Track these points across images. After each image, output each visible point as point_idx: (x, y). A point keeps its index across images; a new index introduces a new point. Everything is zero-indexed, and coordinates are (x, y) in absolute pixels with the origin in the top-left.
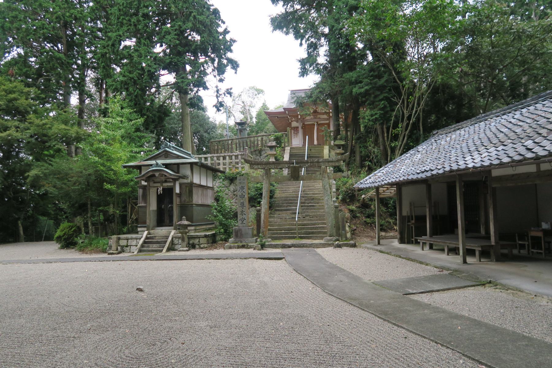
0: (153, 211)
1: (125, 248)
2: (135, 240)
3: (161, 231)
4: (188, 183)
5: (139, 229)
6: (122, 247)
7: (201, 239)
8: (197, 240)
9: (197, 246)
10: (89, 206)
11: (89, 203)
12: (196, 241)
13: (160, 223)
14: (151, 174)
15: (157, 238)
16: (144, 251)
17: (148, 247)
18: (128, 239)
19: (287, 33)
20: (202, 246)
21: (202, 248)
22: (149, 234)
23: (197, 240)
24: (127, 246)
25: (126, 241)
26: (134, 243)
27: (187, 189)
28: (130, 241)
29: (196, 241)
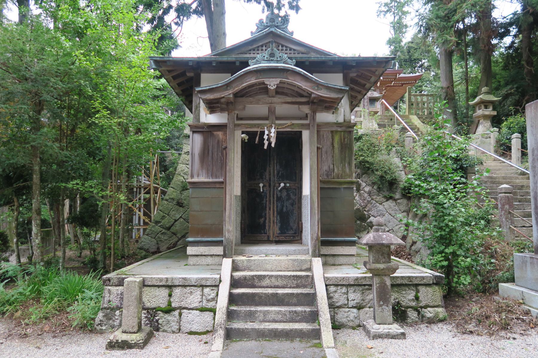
0: (236, 196)
1: (161, 318)
2: (198, 292)
3: (271, 260)
4: (338, 124)
5: (190, 250)
6: (152, 312)
7: (422, 289)
8: (411, 295)
9: (412, 315)
10: (36, 178)
11: (37, 168)
12: (407, 297)
13: (253, 232)
14: (253, 80)
15: (266, 282)
16: (243, 334)
17: (251, 316)
18: (170, 287)
19: (292, 33)
20: (429, 313)
21: (431, 321)
22: (235, 268)
23: (411, 295)
24: (169, 310)
25: (165, 292)
26: (194, 298)
27: (337, 139)
28: (177, 291)
29: (407, 297)
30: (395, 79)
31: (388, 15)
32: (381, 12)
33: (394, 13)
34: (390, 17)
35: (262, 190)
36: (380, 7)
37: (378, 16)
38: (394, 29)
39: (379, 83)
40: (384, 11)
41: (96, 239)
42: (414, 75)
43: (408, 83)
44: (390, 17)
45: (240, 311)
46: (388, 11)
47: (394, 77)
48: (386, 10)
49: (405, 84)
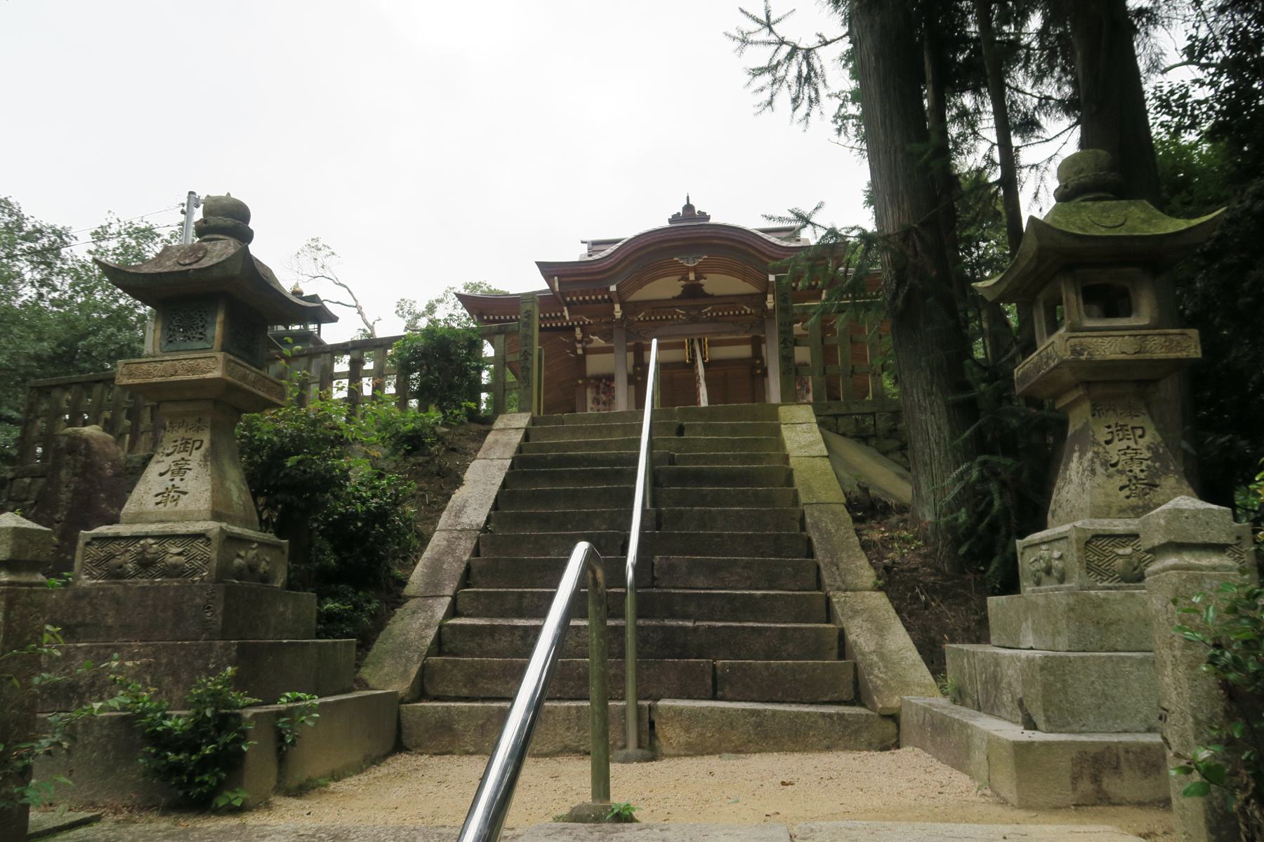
32: (846, 118)
36: (842, 106)
37: (839, 130)
39: (770, 297)
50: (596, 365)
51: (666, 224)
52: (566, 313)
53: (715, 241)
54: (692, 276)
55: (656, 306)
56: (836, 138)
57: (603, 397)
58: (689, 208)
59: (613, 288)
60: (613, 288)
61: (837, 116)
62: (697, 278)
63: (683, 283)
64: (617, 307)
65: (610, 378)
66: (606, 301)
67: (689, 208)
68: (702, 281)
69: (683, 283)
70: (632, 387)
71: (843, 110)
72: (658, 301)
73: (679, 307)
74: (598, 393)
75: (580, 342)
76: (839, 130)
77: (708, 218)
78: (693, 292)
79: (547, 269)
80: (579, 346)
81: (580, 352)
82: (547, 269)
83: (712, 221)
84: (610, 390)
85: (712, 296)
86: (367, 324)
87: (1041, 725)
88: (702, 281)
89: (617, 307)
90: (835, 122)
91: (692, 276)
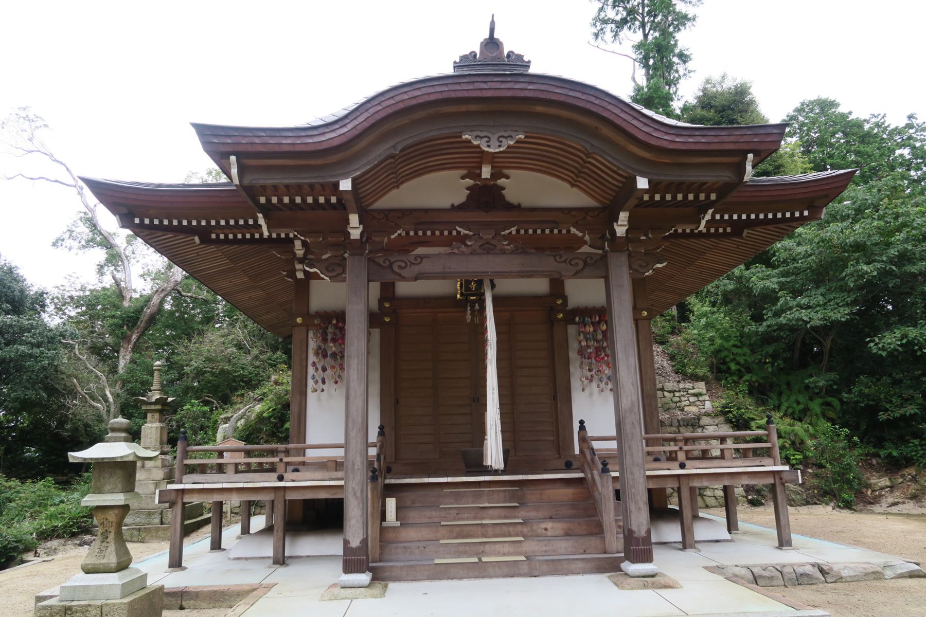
30: (724, 190)
31: (625, 32)
32: (605, 22)
33: (643, 25)
34: (633, 36)
35: (577, 451)
36: (601, 9)
37: (596, 35)
38: (646, 66)
39: (623, 216)
40: (614, 21)
41: (767, 513)
42: (823, 175)
43: (766, 221)
44: (633, 36)
45: (267, 442)
46: (624, 21)
47: (726, 176)
48: (618, 18)
49: (749, 224)
50: (325, 294)
51: (450, 71)
52: (261, 221)
53: (540, 109)
54: (486, 172)
55: (423, 218)
56: (593, 41)
57: (332, 348)
58: (492, 43)
59: (346, 185)
60: (346, 185)
61: (596, 19)
62: (496, 175)
63: (469, 182)
64: (354, 219)
65: (340, 317)
66: (333, 207)
67: (492, 43)
68: (502, 181)
69: (469, 182)
70: (376, 332)
71: (603, 14)
72: (426, 211)
73: (461, 224)
74: (325, 340)
75: (301, 261)
76: (596, 35)
77: (527, 65)
78: (486, 198)
79: (218, 141)
80: (298, 266)
81: (300, 275)
82: (218, 141)
83: (533, 70)
84: (340, 337)
85: (518, 207)
86: (87, 207)
87: (318, 186)
88: (502, 181)
89: (354, 219)
90: (595, 25)
91: (486, 172)
